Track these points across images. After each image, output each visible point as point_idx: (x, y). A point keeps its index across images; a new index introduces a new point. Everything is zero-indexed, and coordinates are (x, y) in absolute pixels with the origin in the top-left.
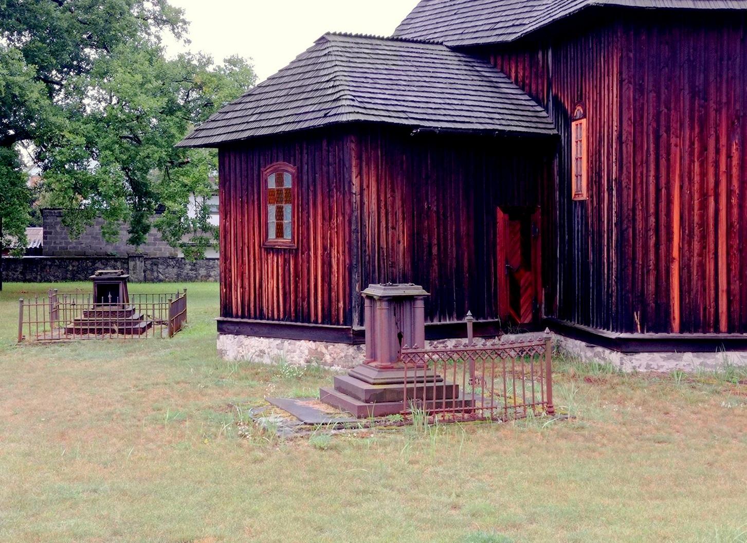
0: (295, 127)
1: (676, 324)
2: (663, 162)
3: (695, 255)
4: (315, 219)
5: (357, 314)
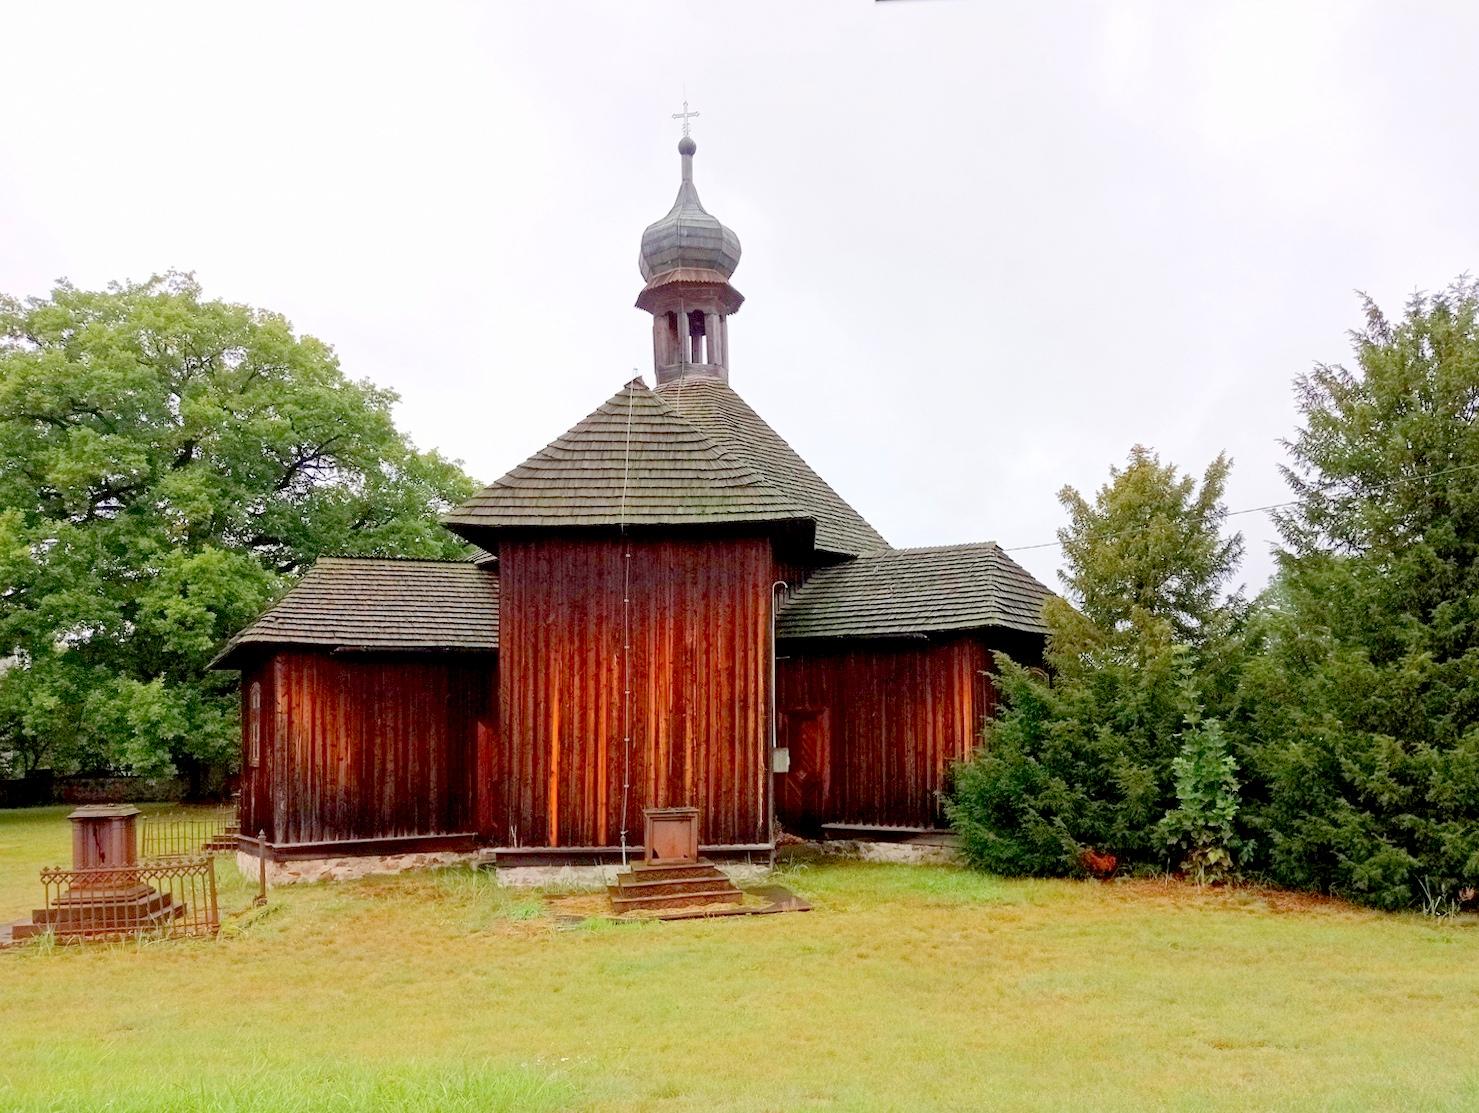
1: (553, 838)
2: (542, 676)
3: (574, 768)
4: (767, 729)
5: (281, 831)
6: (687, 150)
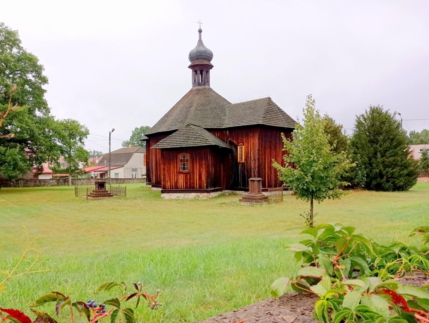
1: (205, 187)
6: (200, 31)
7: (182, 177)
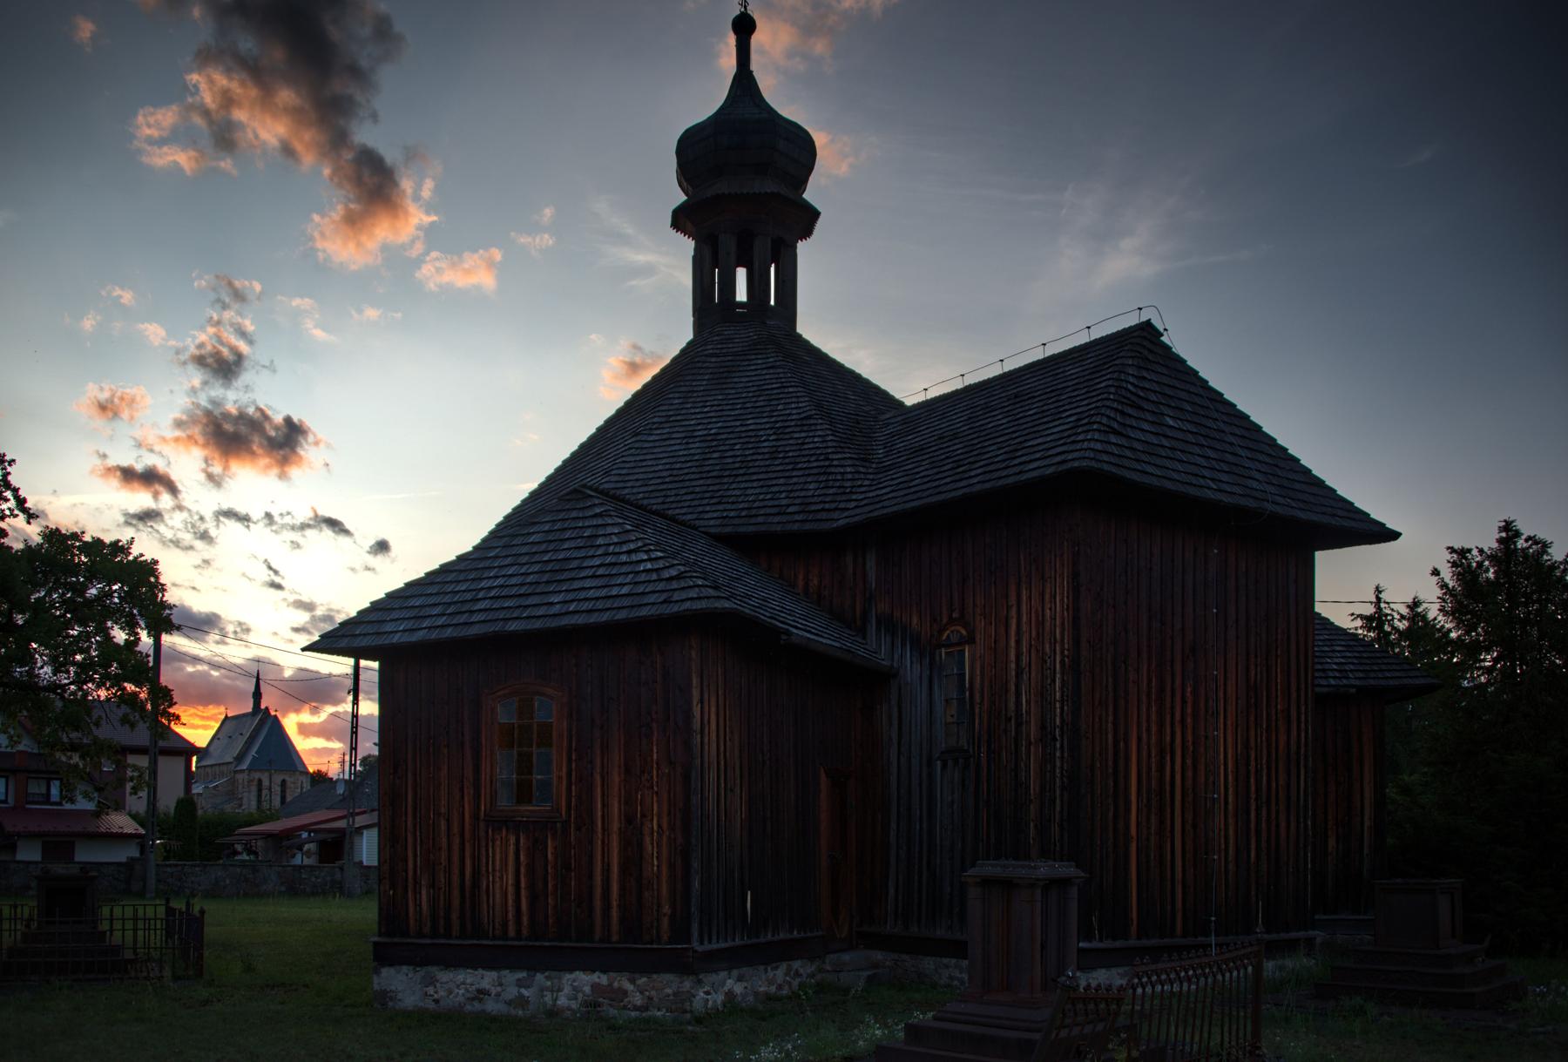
0: (615, 615)
7: (512, 848)
